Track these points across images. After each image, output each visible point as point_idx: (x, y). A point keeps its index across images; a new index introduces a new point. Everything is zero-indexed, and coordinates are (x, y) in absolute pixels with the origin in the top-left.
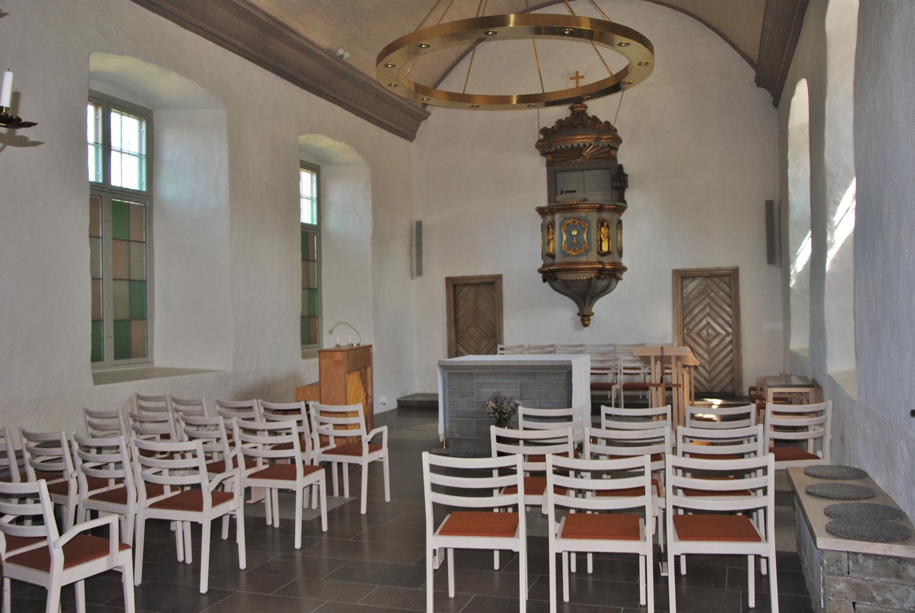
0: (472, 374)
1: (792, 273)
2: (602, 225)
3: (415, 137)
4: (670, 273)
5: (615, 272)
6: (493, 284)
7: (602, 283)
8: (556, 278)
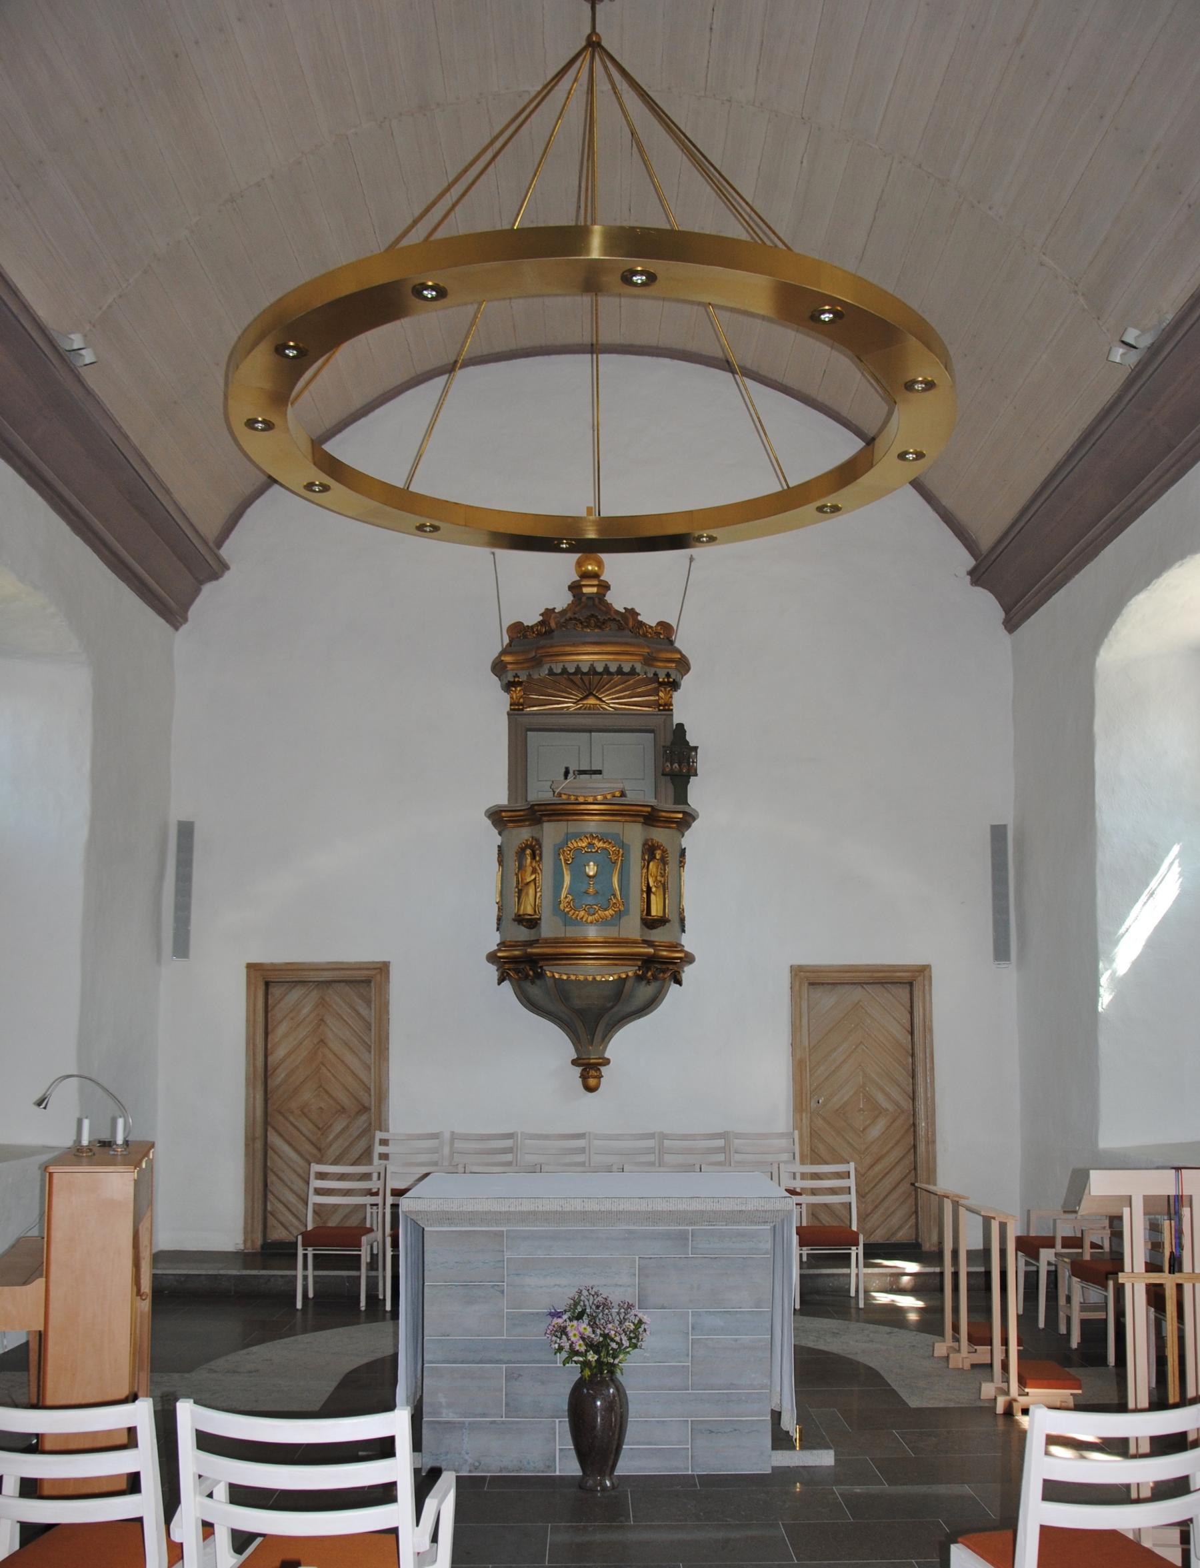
0: (500, 1234)
1: (1104, 980)
2: (652, 857)
3: (186, 620)
4: (785, 979)
5: (661, 967)
6: (367, 982)
7: (645, 991)
8: (540, 976)
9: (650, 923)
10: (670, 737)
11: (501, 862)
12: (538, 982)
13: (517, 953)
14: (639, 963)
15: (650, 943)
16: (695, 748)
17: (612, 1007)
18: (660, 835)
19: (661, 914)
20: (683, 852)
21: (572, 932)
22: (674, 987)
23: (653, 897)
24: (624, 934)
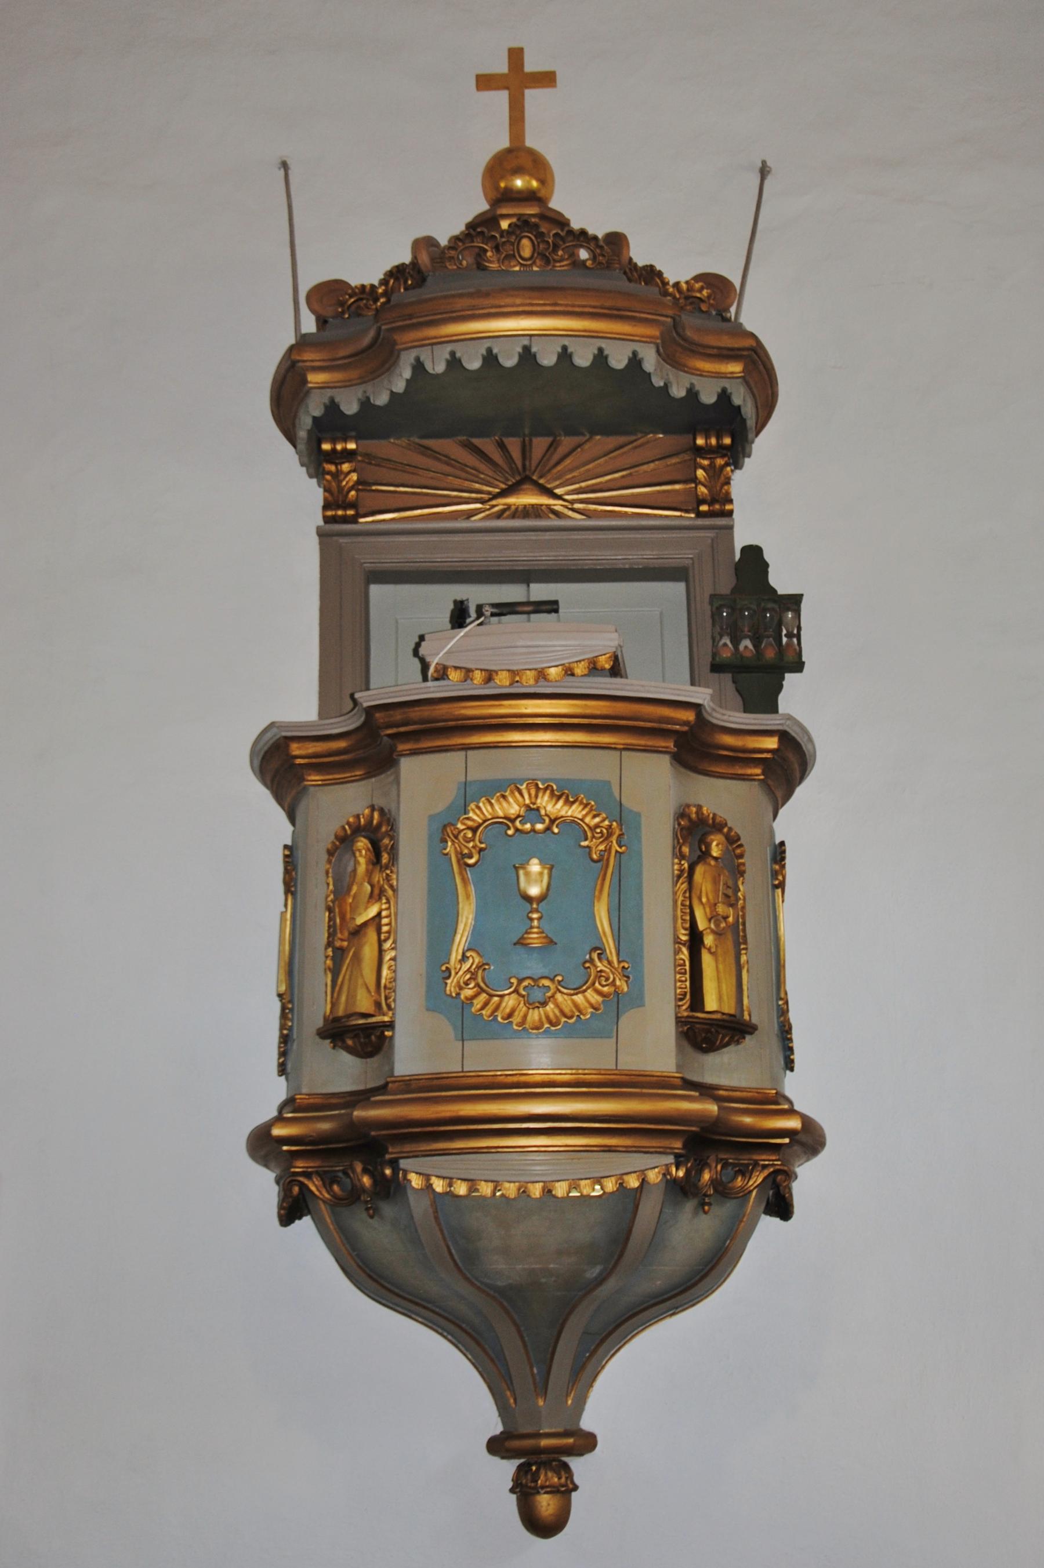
5: (737, 1159)
8: (391, 1189)
9: (704, 1033)
10: (726, 584)
11: (290, 885)
12: (388, 1209)
13: (325, 1126)
14: (678, 1144)
15: (706, 1091)
16: (794, 601)
17: (601, 1280)
18: (721, 797)
19: (729, 1008)
20: (779, 853)
21: (482, 1058)
22: (768, 1223)
23: (707, 959)
24: (631, 1062)
